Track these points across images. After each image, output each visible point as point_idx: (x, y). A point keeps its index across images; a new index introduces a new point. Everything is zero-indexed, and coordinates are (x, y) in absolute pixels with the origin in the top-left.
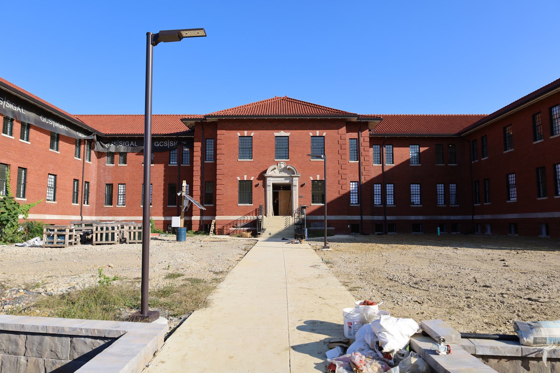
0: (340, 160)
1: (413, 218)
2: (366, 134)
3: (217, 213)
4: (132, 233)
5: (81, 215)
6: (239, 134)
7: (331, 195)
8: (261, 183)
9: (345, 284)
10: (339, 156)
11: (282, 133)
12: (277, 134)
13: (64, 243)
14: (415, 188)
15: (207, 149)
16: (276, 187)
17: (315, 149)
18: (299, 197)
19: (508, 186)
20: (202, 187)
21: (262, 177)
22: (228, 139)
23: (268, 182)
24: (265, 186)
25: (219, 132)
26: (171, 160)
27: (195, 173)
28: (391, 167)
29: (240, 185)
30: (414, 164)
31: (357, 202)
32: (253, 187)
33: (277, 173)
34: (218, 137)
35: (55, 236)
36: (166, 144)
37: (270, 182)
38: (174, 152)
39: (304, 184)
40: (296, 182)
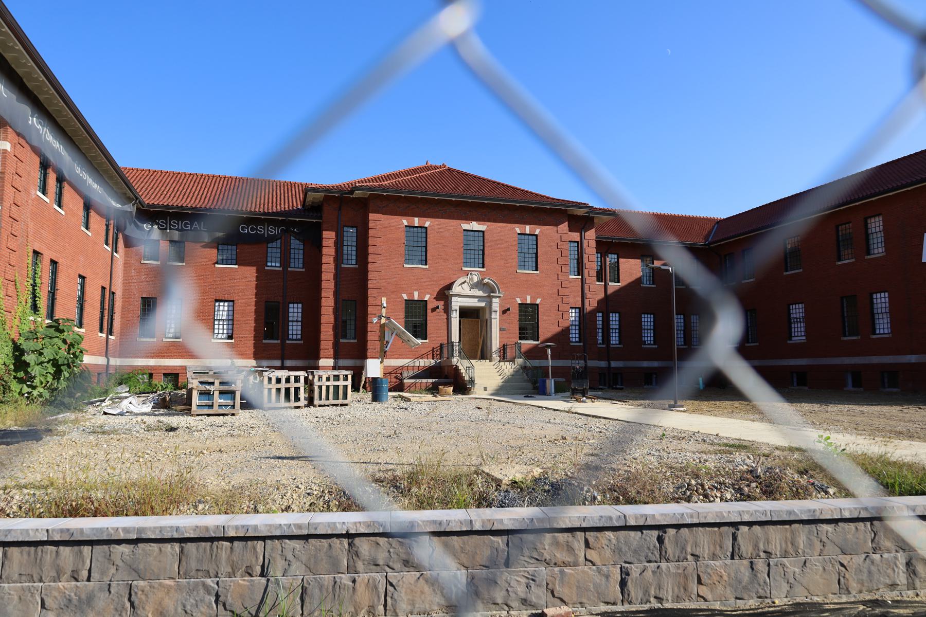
0: (560, 273)
1: (645, 364)
2: (591, 235)
3: (369, 354)
4: (324, 389)
5: (106, 356)
6: (405, 223)
7: (548, 327)
8: (441, 304)
9: (283, 511)
10: (558, 267)
11: (475, 226)
12: (466, 226)
13: (233, 407)
14: (647, 320)
15: (345, 243)
16: (465, 313)
17: (469, 252)
18: (500, 329)
19: (789, 321)
20: (336, 311)
21: (444, 295)
22: (387, 229)
23: (453, 304)
24: (447, 310)
25: (372, 216)
26: (269, 259)
27: (324, 285)
28: (617, 288)
29: (407, 308)
30: (646, 284)
31: (299, 337)
32: (429, 311)
33: (466, 290)
34: (371, 224)
35: (217, 393)
36: (261, 230)
37: (457, 303)
38: (274, 245)
39: (508, 309)
40: (496, 304)
